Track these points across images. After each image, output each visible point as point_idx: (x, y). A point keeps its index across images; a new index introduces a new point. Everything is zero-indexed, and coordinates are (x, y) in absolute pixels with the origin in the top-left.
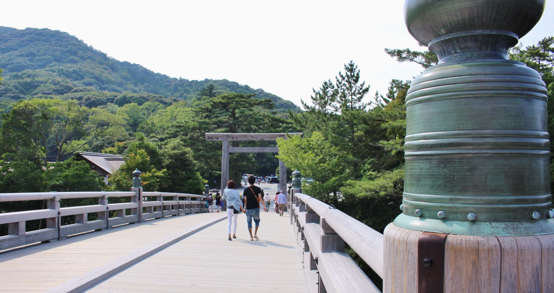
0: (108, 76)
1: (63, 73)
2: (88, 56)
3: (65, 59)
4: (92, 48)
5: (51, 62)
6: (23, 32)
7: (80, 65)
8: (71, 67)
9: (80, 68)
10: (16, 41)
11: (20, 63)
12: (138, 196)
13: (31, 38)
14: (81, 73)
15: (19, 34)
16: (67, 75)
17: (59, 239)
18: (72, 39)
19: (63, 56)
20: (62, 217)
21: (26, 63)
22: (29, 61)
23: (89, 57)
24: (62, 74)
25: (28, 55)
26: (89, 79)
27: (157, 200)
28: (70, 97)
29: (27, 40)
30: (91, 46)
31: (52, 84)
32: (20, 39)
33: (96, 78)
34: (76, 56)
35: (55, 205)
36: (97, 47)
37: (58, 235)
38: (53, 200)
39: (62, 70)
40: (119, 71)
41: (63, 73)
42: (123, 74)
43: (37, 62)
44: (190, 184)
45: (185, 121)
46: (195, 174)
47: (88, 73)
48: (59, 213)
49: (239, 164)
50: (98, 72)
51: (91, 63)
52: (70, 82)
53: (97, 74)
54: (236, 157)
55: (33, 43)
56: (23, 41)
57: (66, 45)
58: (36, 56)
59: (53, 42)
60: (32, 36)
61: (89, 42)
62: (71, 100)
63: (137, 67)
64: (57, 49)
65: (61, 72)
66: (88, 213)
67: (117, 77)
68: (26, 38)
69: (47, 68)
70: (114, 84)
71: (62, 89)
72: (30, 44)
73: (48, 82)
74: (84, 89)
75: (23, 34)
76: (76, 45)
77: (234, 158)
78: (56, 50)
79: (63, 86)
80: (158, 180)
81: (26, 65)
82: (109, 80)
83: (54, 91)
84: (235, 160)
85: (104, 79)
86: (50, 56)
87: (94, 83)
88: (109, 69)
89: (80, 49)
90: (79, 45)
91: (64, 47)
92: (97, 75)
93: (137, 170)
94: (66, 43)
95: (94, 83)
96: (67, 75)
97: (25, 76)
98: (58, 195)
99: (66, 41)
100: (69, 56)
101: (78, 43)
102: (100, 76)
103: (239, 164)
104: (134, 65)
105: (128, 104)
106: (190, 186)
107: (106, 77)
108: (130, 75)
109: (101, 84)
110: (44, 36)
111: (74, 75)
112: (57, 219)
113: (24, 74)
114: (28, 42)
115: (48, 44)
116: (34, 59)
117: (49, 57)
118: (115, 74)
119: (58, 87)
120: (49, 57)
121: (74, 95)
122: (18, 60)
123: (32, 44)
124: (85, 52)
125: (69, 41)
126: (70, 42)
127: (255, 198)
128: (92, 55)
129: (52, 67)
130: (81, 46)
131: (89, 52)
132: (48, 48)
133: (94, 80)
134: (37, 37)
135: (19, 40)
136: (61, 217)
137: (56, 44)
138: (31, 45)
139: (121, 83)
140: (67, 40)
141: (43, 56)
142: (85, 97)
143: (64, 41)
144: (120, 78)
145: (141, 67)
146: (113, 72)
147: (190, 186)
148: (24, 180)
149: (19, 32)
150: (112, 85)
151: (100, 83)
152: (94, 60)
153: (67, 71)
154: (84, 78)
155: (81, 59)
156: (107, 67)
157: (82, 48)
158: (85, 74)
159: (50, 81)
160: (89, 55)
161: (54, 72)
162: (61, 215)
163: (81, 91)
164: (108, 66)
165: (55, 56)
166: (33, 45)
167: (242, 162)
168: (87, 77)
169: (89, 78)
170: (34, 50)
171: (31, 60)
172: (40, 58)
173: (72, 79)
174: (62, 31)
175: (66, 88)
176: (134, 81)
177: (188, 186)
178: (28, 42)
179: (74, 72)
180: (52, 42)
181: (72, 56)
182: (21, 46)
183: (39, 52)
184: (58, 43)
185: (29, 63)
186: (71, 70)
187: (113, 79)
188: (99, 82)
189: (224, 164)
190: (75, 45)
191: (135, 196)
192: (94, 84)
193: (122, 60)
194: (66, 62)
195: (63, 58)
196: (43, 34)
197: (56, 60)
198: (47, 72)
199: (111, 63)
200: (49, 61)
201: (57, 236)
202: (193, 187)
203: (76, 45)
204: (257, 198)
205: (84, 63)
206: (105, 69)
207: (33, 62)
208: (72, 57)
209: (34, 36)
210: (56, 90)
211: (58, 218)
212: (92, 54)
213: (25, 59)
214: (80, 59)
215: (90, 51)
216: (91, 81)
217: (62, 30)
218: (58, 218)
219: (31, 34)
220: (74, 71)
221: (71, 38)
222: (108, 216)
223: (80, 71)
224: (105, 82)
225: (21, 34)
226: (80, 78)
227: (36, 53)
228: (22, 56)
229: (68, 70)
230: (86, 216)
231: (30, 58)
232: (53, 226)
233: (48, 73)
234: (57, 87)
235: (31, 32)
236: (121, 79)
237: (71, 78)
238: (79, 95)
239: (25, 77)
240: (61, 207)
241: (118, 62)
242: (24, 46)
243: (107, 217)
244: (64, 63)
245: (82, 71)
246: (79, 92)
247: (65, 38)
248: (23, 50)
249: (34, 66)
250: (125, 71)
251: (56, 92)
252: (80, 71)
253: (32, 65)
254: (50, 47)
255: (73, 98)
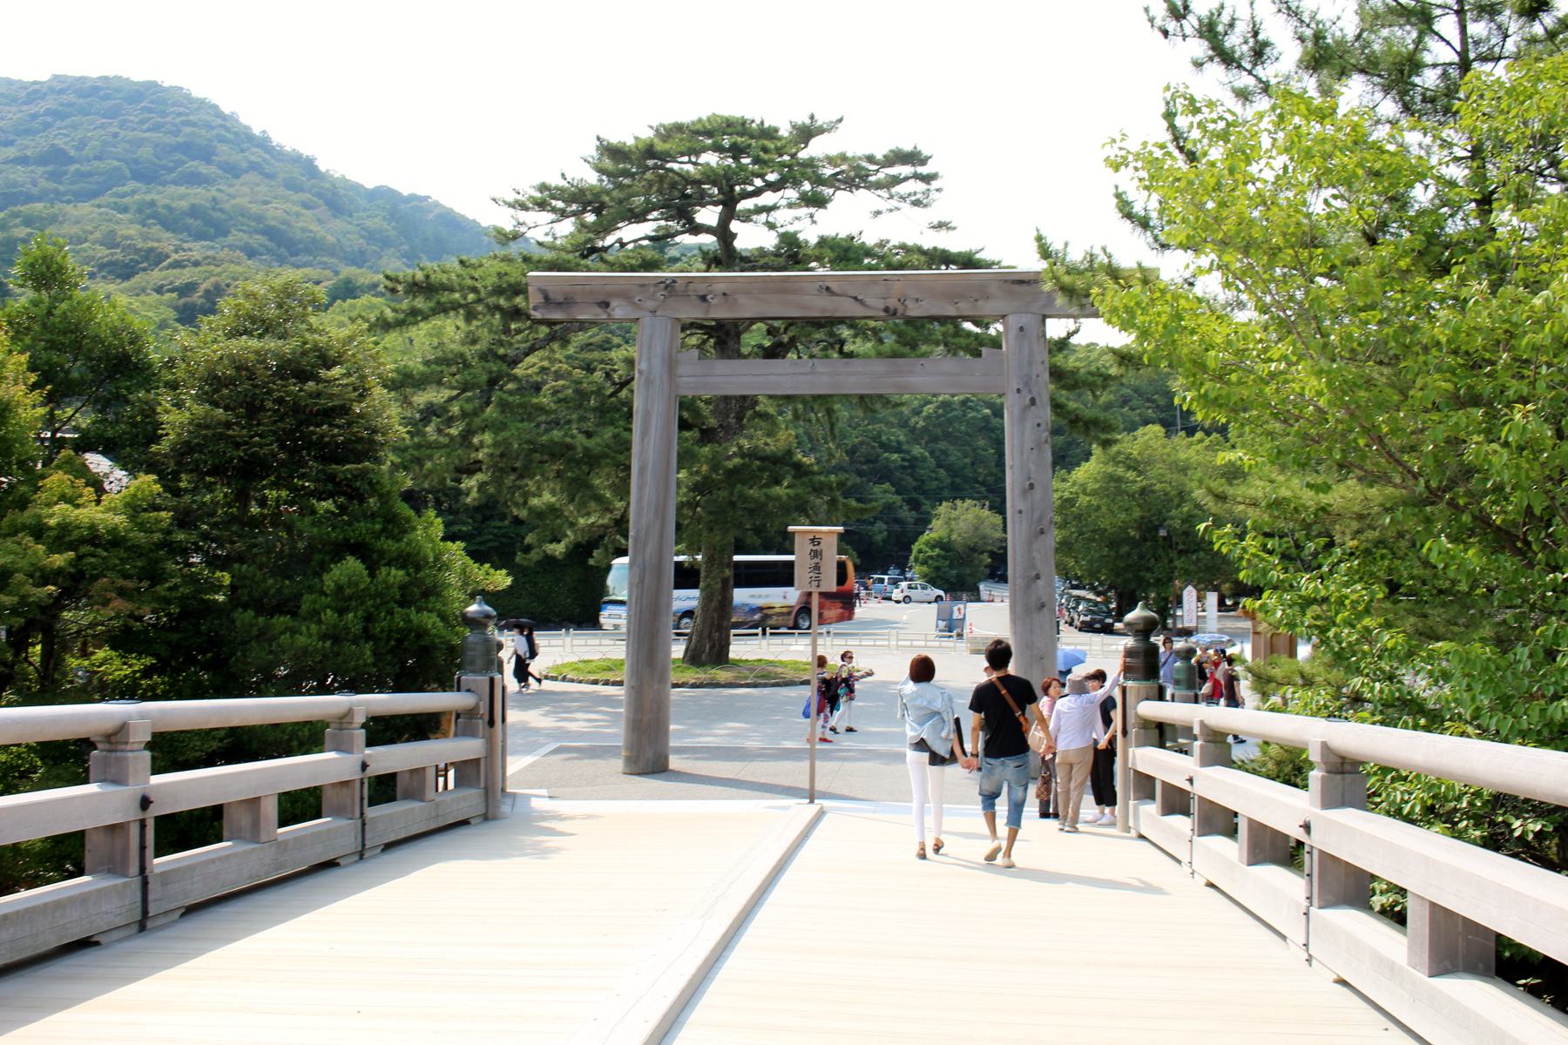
0: (314, 227)
1: (155, 216)
2: (251, 162)
3: (171, 170)
4: (268, 139)
5: (121, 181)
6: (37, 87)
7: (219, 190)
8: (182, 197)
9: (214, 199)
10: (10, 115)
11: (15, 184)
12: (484, 709)
13: (62, 105)
14: (217, 215)
15: (23, 94)
16: (170, 222)
17: (142, 925)
18: (199, 108)
19: (164, 162)
20: (162, 821)
21: (35, 184)
22: (47, 179)
23: (254, 167)
24: (149, 217)
25: (42, 160)
26: (245, 237)
27: (328, 742)
28: (151, 286)
29: (48, 113)
30: (264, 132)
31: (102, 244)
32: (25, 108)
33: (270, 232)
34: (208, 162)
35: (121, 762)
36: (289, 135)
37: (139, 911)
38: (117, 736)
39: (152, 204)
40: (355, 214)
41: (155, 216)
42: (368, 223)
43: (72, 183)
44: (343, 599)
45: (462, 262)
46: (394, 526)
47: (242, 215)
48: (145, 803)
49: (752, 492)
50: (279, 213)
51: (258, 185)
52: (166, 241)
53: (275, 218)
54: (737, 460)
55: (68, 121)
56: (34, 117)
57: (174, 125)
58: (71, 160)
59: (136, 116)
60: (65, 98)
61: (255, 119)
62: (156, 296)
63: (424, 204)
64: (143, 139)
65: (148, 211)
66: (280, 795)
67: (349, 233)
68: (41, 107)
69: (106, 198)
70: (333, 255)
71: (131, 260)
72: (59, 124)
73: (91, 237)
74: (206, 258)
75: (36, 92)
76: (213, 128)
77: (730, 464)
78: (139, 143)
79: (138, 251)
80: (59, 560)
81: (35, 191)
82: (314, 240)
83: (102, 267)
84: (731, 473)
85: (299, 235)
86: (119, 160)
87: (262, 249)
88: (318, 207)
89: (222, 140)
90: (221, 126)
91: (171, 133)
92: (273, 223)
93: (480, 604)
94: (178, 120)
95: (262, 249)
96: (170, 222)
97: (18, 221)
98: (142, 715)
99: (180, 115)
100: (184, 163)
101: (219, 121)
102: (283, 227)
103: (752, 492)
104: (413, 197)
105: (349, 301)
106: (341, 612)
107: (303, 229)
108: (394, 228)
109: (286, 254)
110: (107, 97)
111: (190, 221)
112: (134, 831)
113: (16, 215)
114: (49, 119)
115: (116, 122)
116: (66, 173)
117: (116, 163)
118: (339, 224)
119: (119, 255)
120: (116, 163)
121: (165, 279)
122: (12, 176)
123: (63, 124)
124: (242, 151)
125: (187, 115)
126: (191, 118)
127: (1017, 719)
128: (265, 160)
129: (124, 195)
130: (228, 130)
131: (255, 150)
132: (115, 135)
133: (262, 239)
134: (81, 101)
135: (21, 111)
136: (157, 818)
137: (142, 122)
138: (60, 128)
139: (362, 253)
140: (182, 109)
141: (96, 163)
142: (204, 286)
143: (173, 113)
144: (356, 236)
145: (437, 205)
146: (335, 216)
147: (341, 612)
148: (195, 656)
149: (26, 88)
150: (325, 259)
151: (282, 249)
152: (269, 176)
153: (167, 207)
154: (226, 233)
155: (226, 171)
156: (315, 199)
157: (230, 136)
158: (231, 219)
159: (97, 235)
160: (253, 158)
161: (125, 210)
162: (156, 810)
163: (196, 264)
164: (320, 196)
165: (136, 161)
166: (66, 128)
167: (767, 486)
168: (241, 230)
169: (244, 232)
170: (66, 143)
171: (55, 177)
172: (85, 168)
173: (184, 235)
174: (165, 85)
175: (146, 258)
176: (406, 247)
177: (329, 615)
178: (49, 119)
179: (194, 212)
180: (132, 118)
181: (195, 163)
182: (27, 132)
183: (82, 149)
184: (149, 119)
185: (43, 183)
186: (184, 204)
187: (330, 239)
188: (279, 246)
189: (642, 470)
190: (209, 126)
191: (471, 713)
192: (261, 254)
193: (370, 183)
194: (175, 182)
195: (165, 168)
196: (102, 93)
197: (137, 176)
198: (96, 209)
199: (327, 185)
200: (115, 178)
201: (139, 917)
202: (369, 618)
203: (213, 128)
204: (1022, 719)
205: (232, 186)
206: (306, 206)
207: (60, 183)
208: (193, 165)
209: (72, 98)
210: (110, 264)
211: (143, 825)
212: (267, 156)
213: (32, 172)
214: (220, 172)
215: (258, 146)
216: (251, 241)
217: (168, 81)
218: (143, 825)
219: (62, 92)
220: (193, 206)
221: (195, 106)
222: (366, 801)
223: (213, 209)
224: (301, 246)
225: (28, 94)
226: (212, 231)
227: (72, 153)
228: (23, 161)
229: (174, 205)
230: (271, 809)
231: (50, 168)
232: (114, 866)
233: (101, 214)
234: (112, 254)
235: (64, 85)
236: (361, 241)
237: (181, 233)
238: (185, 276)
239: (16, 226)
240: (156, 770)
241: (357, 187)
242: (37, 132)
243: (143, 848)
244: (164, 184)
245: (221, 210)
246: (185, 267)
247: (176, 104)
248: (33, 144)
249: (65, 193)
250: (377, 216)
251: (110, 272)
252: (213, 209)
253: (56, 192)
254: (122, 133)
255: (162, 286)
